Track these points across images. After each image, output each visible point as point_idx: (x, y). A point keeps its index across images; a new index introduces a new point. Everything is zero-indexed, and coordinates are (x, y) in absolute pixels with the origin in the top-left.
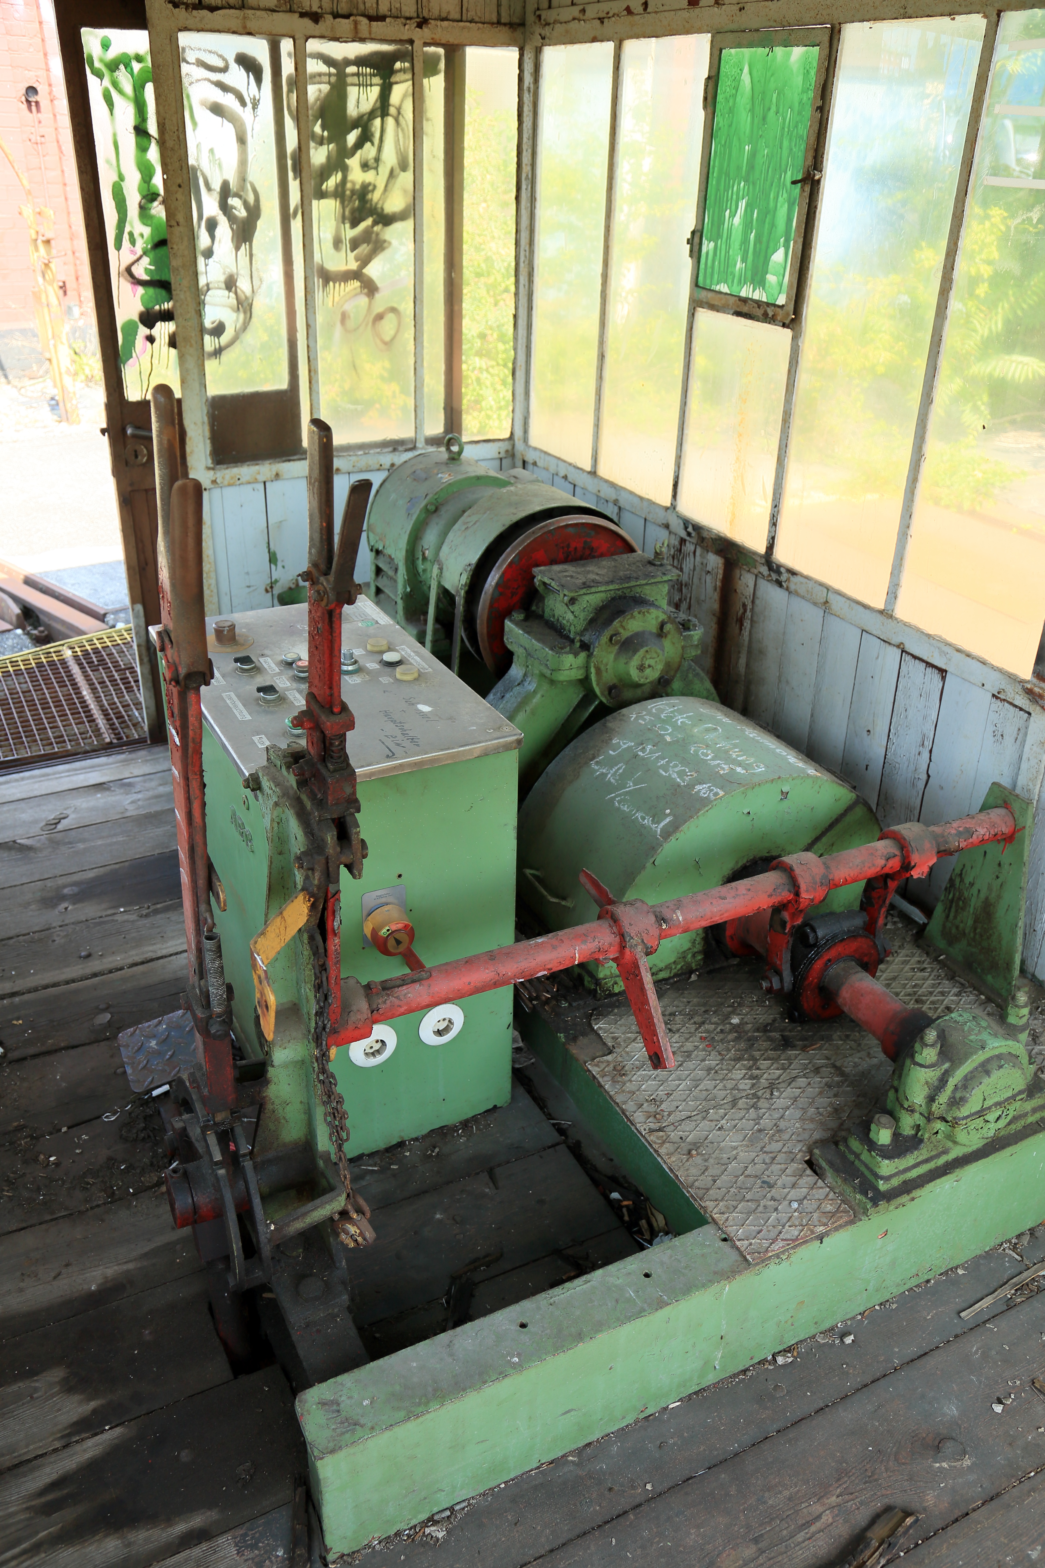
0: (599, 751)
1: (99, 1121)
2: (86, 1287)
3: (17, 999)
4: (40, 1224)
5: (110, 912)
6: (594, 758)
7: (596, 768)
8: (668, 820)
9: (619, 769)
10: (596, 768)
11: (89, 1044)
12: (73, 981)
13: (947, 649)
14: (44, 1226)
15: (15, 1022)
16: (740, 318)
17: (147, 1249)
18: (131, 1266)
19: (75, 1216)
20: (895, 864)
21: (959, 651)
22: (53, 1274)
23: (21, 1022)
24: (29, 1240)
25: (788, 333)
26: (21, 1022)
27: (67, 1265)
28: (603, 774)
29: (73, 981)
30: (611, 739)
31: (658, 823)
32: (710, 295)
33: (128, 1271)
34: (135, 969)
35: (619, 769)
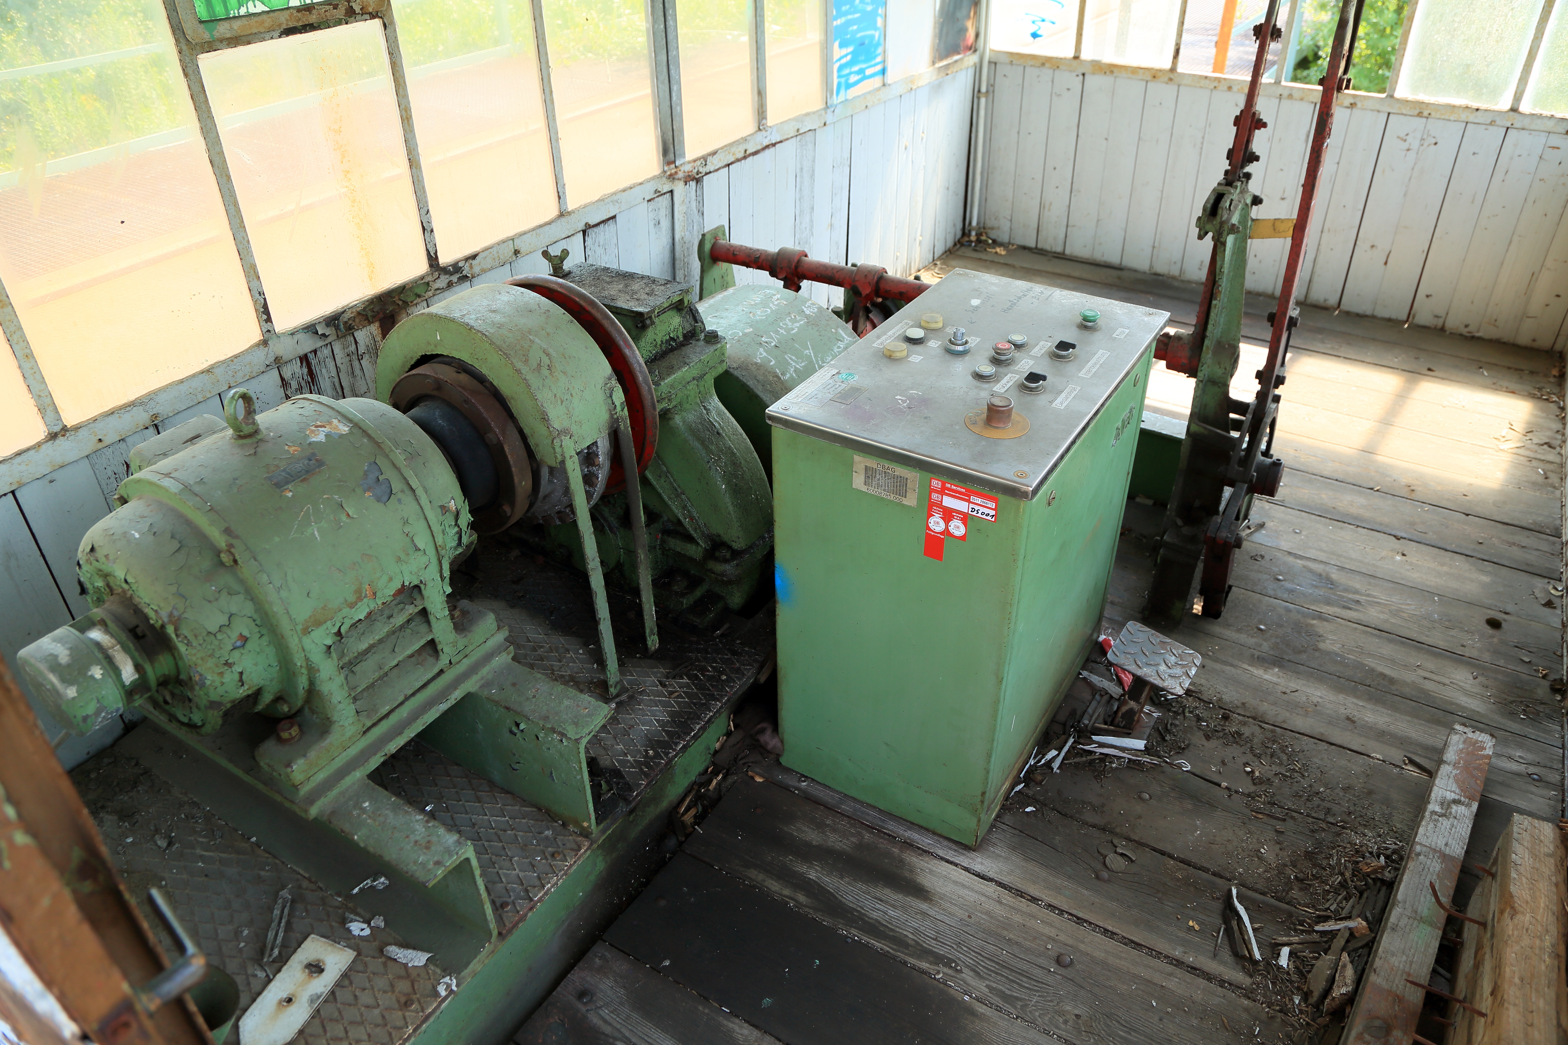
0: (769, 372)
1: (1194, 771)
2: (1281, 674)
3: (1177, 953)
4: (1286, 729)
5: (981, 1009)
6: (777, 377)
7: (788, 375)
8: (841, 331)
9: (791, 359)
10: (788, 375)
11: (1148, 846)
12: (1106, 931)
13: (615, 198)
14: (1285, 726)
15: (1197, 927)
16: (291, 37)
17: (1229, 668)
18: (1246, 666)
19: (1258, 719)
20: (173, 672)
21: (624, 190)
22: (1296, 694)
23: (1191, 923)
24: (1300, 723)
25: (377, 23)
26: (1191, 923)
27: (1285, 693)
28: (795, 371)
29: (1106, 931)
30: (756, 364)
31: (843, 338)
32: (236, 24)
33: (1249, 665)
34: (1036, 893)
35: (791, 359)
